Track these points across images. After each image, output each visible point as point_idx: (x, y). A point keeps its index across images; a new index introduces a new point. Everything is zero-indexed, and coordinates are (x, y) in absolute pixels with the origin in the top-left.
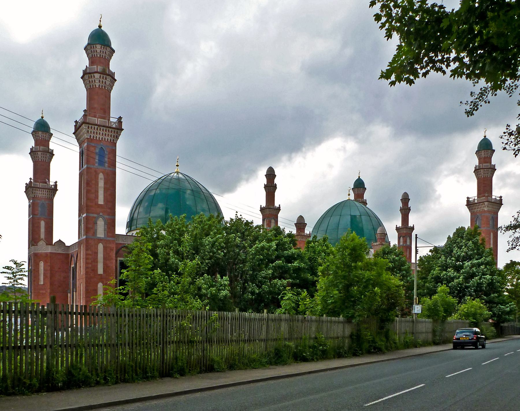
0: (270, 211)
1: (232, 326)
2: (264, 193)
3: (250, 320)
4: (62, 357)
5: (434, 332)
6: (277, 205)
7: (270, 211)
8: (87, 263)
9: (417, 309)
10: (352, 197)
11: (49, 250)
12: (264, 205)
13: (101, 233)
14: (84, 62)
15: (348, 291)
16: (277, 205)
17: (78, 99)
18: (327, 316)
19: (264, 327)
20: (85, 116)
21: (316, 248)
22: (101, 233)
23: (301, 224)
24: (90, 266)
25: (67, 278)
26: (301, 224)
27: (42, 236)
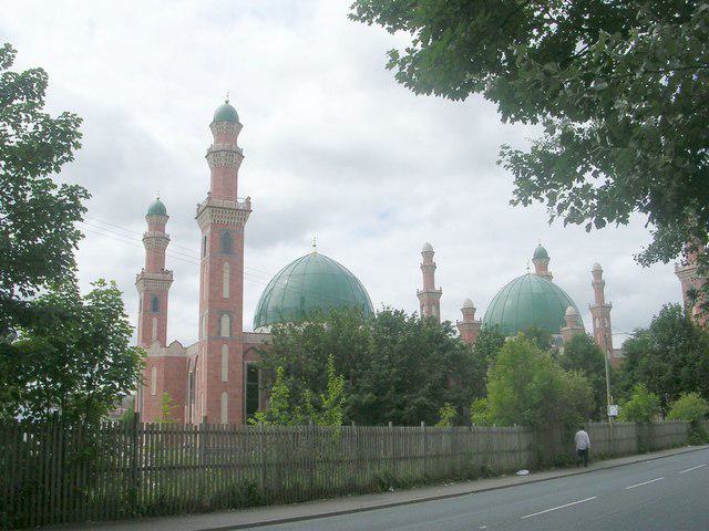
0: (431, 297)
1: (385, 442)
2: (420, 274)
3: (406, 434)
4: (152, 443)
5: (639, 439)
6: (437, 288)
7: (431, 297)
8: (209, 368)
9: (613, 410)
10: (533, 270)
11: (163, 353)
12: (421, 289)
13: (225, 332)
14: (209, 140)
15: (521, 392)
16: (437, 288)
17: (199, 180)
18: (394, 425)
19: (422, 440)
20: (209, 198)
21: (491, 339)
22: (225, 332)
23: (469, 311)
24: (212, 371)
25: (183, 387)
26: (469, 311)
27: (155, 335)
